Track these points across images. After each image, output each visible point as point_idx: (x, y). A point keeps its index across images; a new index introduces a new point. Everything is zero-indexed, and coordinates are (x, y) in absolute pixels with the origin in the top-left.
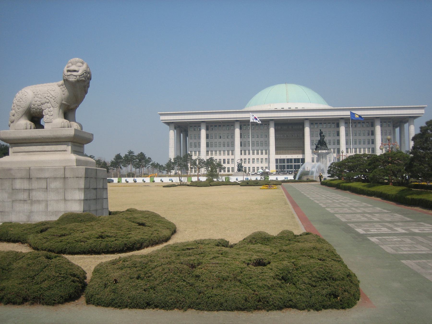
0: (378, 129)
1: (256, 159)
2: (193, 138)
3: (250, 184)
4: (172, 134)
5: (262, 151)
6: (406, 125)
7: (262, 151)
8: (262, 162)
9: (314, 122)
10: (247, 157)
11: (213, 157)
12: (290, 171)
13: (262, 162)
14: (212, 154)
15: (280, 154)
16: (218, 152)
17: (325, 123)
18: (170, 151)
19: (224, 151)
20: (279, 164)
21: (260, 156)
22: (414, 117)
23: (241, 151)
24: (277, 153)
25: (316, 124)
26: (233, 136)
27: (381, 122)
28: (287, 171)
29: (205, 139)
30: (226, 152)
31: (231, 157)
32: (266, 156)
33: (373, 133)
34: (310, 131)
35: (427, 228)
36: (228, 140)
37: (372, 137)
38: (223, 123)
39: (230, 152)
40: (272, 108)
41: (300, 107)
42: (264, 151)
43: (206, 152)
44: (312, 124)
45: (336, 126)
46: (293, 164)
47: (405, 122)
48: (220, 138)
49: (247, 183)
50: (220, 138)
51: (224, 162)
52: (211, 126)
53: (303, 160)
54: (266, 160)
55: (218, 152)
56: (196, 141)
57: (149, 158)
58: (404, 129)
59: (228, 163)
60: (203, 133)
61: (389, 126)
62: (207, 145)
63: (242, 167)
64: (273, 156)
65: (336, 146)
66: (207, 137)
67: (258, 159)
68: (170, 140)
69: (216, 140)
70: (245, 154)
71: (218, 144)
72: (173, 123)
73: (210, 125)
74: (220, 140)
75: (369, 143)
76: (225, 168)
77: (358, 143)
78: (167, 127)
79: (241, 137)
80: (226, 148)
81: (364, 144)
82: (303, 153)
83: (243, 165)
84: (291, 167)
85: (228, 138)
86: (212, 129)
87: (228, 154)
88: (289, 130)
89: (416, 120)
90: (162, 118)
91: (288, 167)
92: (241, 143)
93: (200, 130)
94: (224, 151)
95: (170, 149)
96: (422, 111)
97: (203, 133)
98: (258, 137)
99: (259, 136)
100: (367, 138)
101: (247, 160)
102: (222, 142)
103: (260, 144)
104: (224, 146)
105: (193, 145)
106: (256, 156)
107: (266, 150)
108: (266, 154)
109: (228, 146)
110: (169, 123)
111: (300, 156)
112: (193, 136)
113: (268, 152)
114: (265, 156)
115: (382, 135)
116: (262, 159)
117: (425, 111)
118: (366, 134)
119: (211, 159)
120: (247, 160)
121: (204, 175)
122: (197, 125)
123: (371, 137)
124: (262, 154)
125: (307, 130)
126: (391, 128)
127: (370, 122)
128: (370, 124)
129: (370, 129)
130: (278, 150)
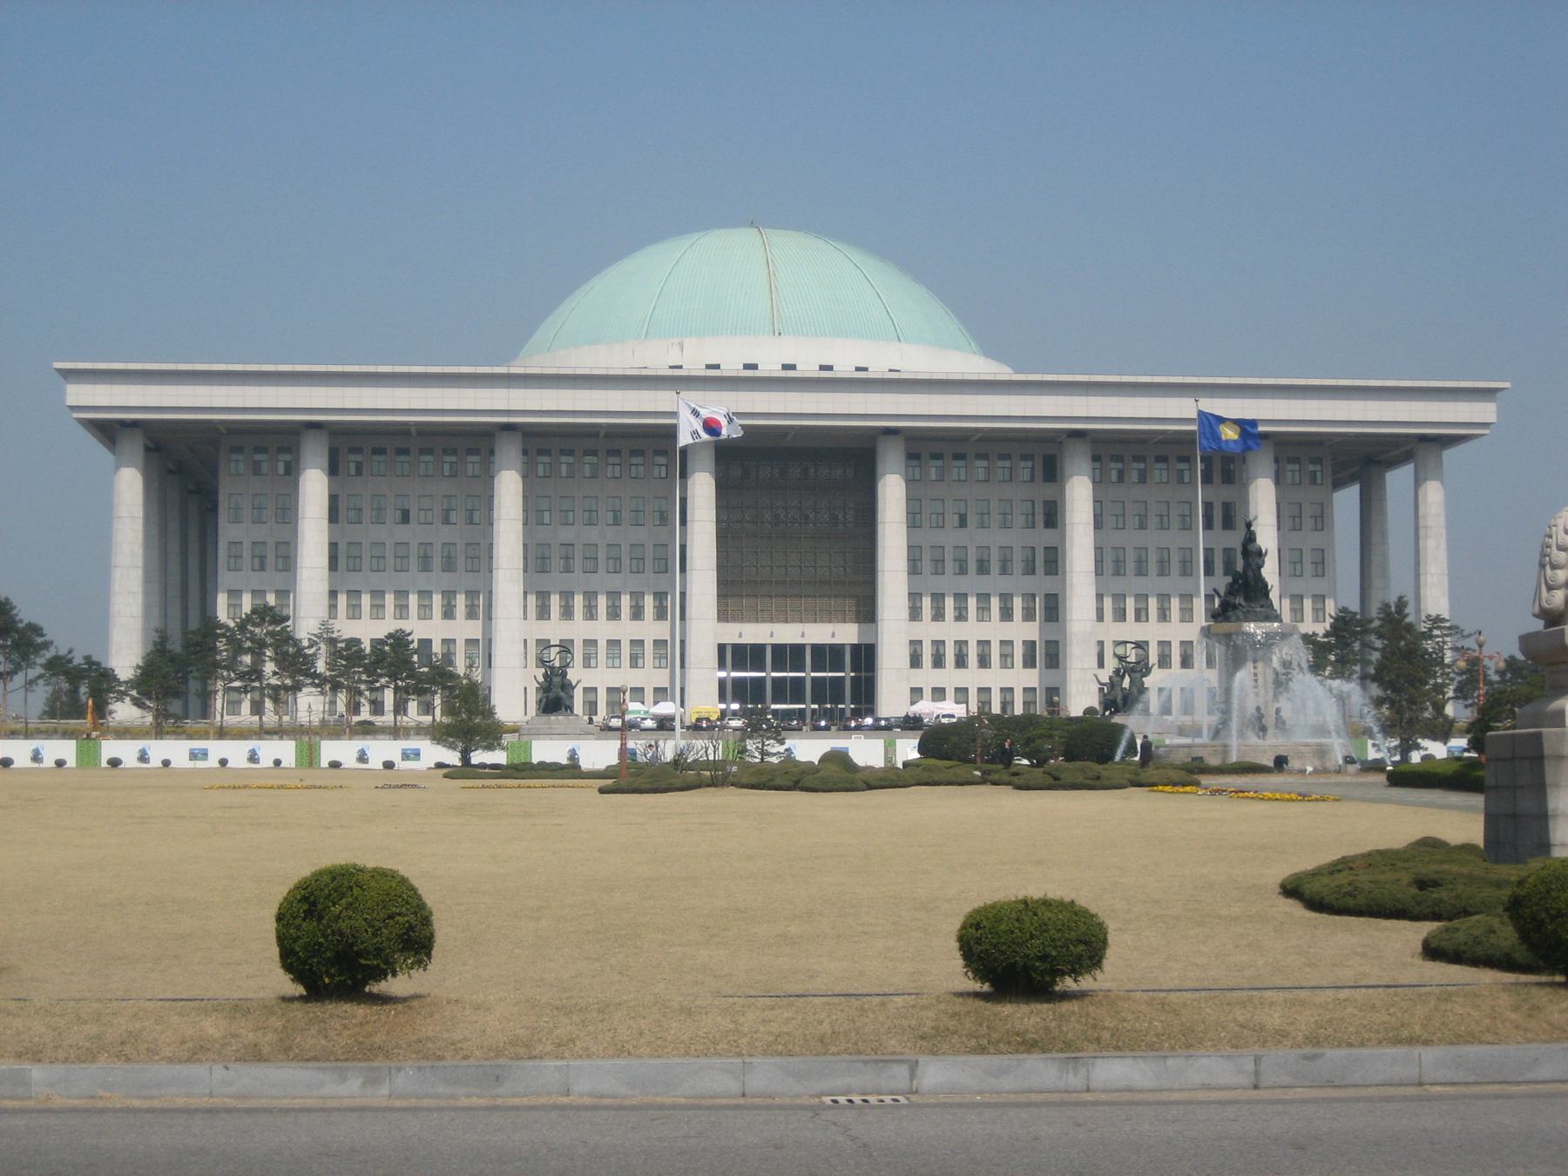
1: (602, 645)
4: (129, 487)
5: (637, 597)
6: (1398, 479)
7: (637, 597)
8: (635, 661)
9: (931, 449)
10: (950, 631)
11: (406, 625)
14: (402, 610)
16: (389, 599)
17: (984, 456)
19: (425, 594)
21: (626, 629)
23: (333, 594)
24: (725, 614)
25: (937, 456)
26: (288, 513)
29: (325, 522)
32: (660, 630)
33: (1053, 516)
34: (1097, 502)
36: (444, 534)
39: (1175, 603)
40: (656, 358)
41: (879, 366)
42: (461, 601)
43: (326, 597)
45: (1039, 473)
47: (1393, 463)
48: (405, 518)
49: (633, 778)
50: (405, 518)
52: (356, 450)
53: (865, 656)
54: (676, 646)
60: (314, 486)
61: (1313, 481)
63: (567, 687)
64: (707, 630)
65: (1041, 583)
67: (614, 644)
70: (938, 615)
71: (389, 553)
73: (357, 447)
74: (403, 533)
77: (1153, 566)
78: (93, 447)
79: (333, 516)
80: (438, 579)
81: (1004, 571)
82: (867, 612)
83: (572, 675)
85: (446, 521)
86: (359, 466)
88: (801, 493)
89: (1450, 455)
90: (81, 395)
91: (782, 690)
92: (333, 546)
94: (425, 594)
96: (1484, 412)
97: (314, 486)
98: (616, 523)
99: (626, 515)
100: (1018, 538)
103: (626, 561)
104: (425, 566)
105: (247, 554)
107: (472, 594)
108: (471, 614)
109: (449, 566)
110: (109, 431)
111: (846, 633)
113: (673, 605)
114: (651, 629)
115: (1098, 524)
116: (638, 643)
117: (1500, 413)
118: (1019, 520)
119: (399, 640)
122: (277, 443)
124: (637, 614)
125: (892, 492)
130: (735, 592)
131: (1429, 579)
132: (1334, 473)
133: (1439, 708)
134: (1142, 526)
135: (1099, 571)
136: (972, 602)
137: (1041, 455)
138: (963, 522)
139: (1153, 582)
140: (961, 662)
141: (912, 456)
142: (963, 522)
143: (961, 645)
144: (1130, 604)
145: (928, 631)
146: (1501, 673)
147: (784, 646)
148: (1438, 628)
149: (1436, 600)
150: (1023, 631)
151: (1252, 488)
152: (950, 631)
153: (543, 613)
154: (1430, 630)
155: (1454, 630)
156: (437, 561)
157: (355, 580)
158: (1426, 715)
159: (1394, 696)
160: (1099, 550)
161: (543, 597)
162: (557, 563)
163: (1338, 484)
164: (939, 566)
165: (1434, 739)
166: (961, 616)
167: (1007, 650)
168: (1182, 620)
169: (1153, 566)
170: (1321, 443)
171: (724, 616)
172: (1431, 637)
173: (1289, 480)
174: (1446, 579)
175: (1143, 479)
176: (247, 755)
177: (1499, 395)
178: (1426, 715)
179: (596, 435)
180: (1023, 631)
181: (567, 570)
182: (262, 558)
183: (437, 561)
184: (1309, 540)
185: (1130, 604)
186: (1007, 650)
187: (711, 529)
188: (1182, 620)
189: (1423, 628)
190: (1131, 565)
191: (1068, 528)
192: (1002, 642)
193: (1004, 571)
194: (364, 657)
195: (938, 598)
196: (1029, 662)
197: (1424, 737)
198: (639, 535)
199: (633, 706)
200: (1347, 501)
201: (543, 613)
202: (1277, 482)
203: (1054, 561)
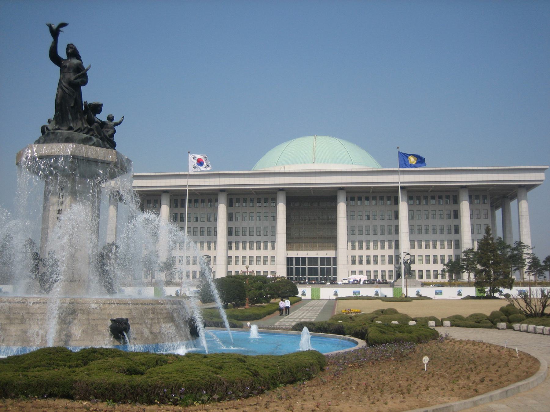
0: (465, 207)
1: (255, 258)
6: (513, 204)
8: (265, 263)
9: (357, 195)
10: (364, 252)
12: (313, 279)
13: (265, 263)
15: (296, 249)
20: (332, 267)
22: (528, 187)
27: (470, 197)
28: (309, 279)
30: (205, 245)
31: (269, 253)
33: (457, 215)
34: (409, 210)
37: (455, 222)
38: (202, 195)
44: (353, 199)
46: (294, 267)
47: (512, 198)
50: (197, 220)
59: (368, 262)
62: (230, 232)
66: (230, 217)
67: (258, 257)
74: (367, 223)
75: (449, 232)
77: (431, 231)
81: (442, 233)
82: (336, 248)
84: (316, 272)
85: (209, 220)
87: (368, 248)
93: (276, 206)
96: (540, 176)
97: (222, 209)
98: (260, 220)
99: (262, 218)
101: (241, 258)
102: (199, 228)
106: (255, 253)
116: (266, 257)
120: (241, 258)
121: (468, 284)
123: (454, 222)
127: (449, 195)
128: (452, 199)
131: (524, 233)
134: (427, 218)
135: (472, 233)
136: (372, 244)
137: (388, 195)
138: (368, 218)
139: (431, 236)
140: (368, 262)
141: (410, 198)
142: (368, 218)
143: (435, 256)
144: (424, 244)
145: (357, 253)
146: (544, 262)
147: (312, 258)
150: (389, 252)
151: (461, 204)
152: (364, 252)
153: (353, 247)
156: (205, 233)
157: (238, 239)
160: (472, 225)
161: (353, 243)
162: (357, 232)
163: (497, 208)
164: (361, 232)
166: (420, 247)
167: (383, 258)
168: (441, 248)
169: (431, 231)
171: (288, 248)
174: (529, 232)
175: (427, 204)
176: (457, 293)
177: (545, 171)
179: (427, 191)
180: (389, 252)
181: (245, 235)
182: (203, 232)
183: (205, 233)
185: (424, 244)
186: (383, 258)
187: (284, 220)
188: (441, 248)
190: (423, 231)
191: (461, 217)
192: (382, 256)
193: (382, 233)
194: (478, 263)
195: (420, 242)
196: (390, 262)
198: (267, 224)
199: (56, 276)
200: (499, 213)
201: (353, 247)
203: (457, 230)
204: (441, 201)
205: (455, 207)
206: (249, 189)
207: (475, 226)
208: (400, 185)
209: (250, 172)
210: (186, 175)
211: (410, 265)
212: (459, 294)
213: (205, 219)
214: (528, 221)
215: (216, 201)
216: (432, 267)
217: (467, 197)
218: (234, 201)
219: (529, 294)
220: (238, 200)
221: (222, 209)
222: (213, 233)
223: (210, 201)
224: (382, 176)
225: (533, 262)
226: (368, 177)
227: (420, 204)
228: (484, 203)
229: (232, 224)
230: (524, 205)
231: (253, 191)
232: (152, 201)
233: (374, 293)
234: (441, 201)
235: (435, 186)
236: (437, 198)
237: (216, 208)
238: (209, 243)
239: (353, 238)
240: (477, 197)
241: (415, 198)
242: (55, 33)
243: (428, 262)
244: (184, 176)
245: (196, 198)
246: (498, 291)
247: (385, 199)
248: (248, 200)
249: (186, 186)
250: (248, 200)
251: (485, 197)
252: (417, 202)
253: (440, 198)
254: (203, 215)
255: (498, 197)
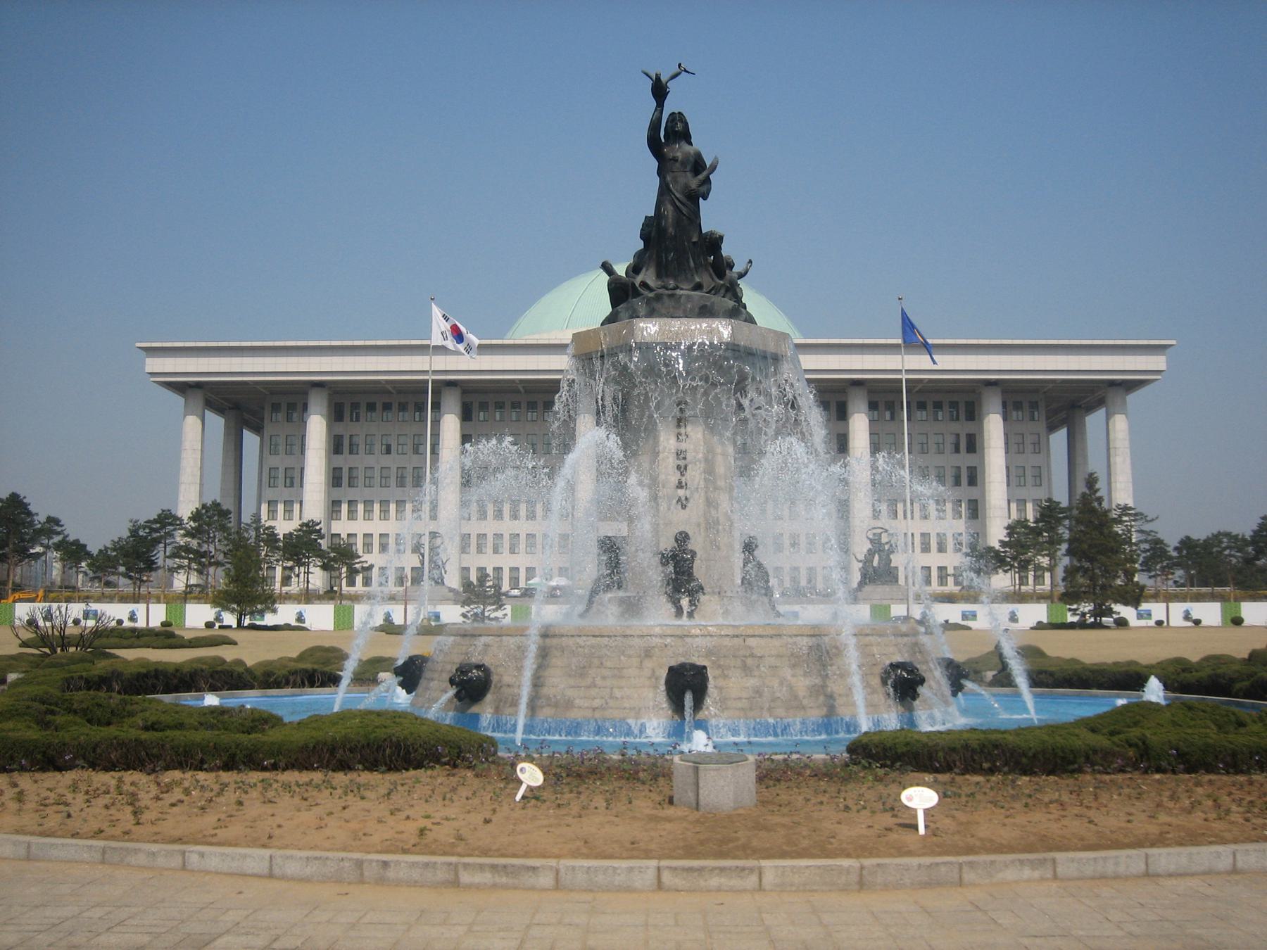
0: (994, 427)
1: (523, 537)
2: (281, 448)
3: (185, 839)
6: (1094, 421)
10: (490, 527)
16: (377, 507)
18: (181, 498)
22: (1129, 385)
26: (298, 445)
27: (1004, 405)
33: (973, 444)
35: (1251, 856)
37: (969, 460)
38: (399, 392)
47: (1090, 409)
48: (388, 451)
50: (388, 451)
51: (368, 547)
55: (377, 507)
56: (290, 461)
57: (50, 520)
58: (1083, 433)
59: (941, 549)
62: (335, 478)
66: (336, 445)
68: (184, 455)
69: (370, 460)
72: (198, 385)
73: (352, 402)
74: (387, 461)
76: (371, 567)
78: (178, 400)
80: (395, 492)
87: (515, 516)
89: (1133, 398)
90: (156, 365)
95: (182, 488)
96: (1157, 362)
97: (317, 428)
100: (951, 460)
101: (490, 538)
102: (377, 468)
110: (181, 388)
112: (281, 441)
118: (949, 447)
120: (490, 538)
123: (965, 460)
126: (1041, 426)
127: (954, 403)
129: (964, 428)
132: (1048, 418)
133: (1129, 574)
141: (873, 406)
146: (1176, 549)
148: (1126, 515)
149: (1121, 491)
151: (986, 421)
154: (1120, 516)
155: (1138, 516)
157: (352, 493)
158: (1119, 582)
159: (1087, 565)
163: (1052, 428)
165: (1126, 604)
170: (1036, 391)
172: (1121, 522)
173: (1014, 417)
176: (1182, 615)
177: (1168, 351)
178: (1119, 582)
184: (1030, 460)
189: (1114, 515)
197: (1116, 602)
200: (1059, 439)
202: (1005, 419)
203: (974, 477)
204: (940, 413)
205: (969, 427)
206: (513, 381)
207: (1013, 470)
208: (904, 377)
209: (506, 342)
210: (428, 346)
211: (888, 555)
212: (1013, 618)
213: (409, 448)
214: (1128, 461)
215: (305, 408)
216: (934, 560)
217: (863, 405)
218: (476, 406)
219: (269, 619)
220: (484, 406)
221: (317, 428)
222: (297, 480)
223: (532, 406)
224: (848, 357)
225: (1152, 549)
226: (854, 356)
227: (892, 418)
228: (1032, 419)
229: (339, 461)
230: (1120, 424)
231: (520, 387)
232: (284, 407)
233: (295, 617)
234: (940, 413)
235: (930, 380)
236: (930, 406)
237: (303, 423)
238: (288, 504)
239: (1022, 493)
240: (1018, 406)
241: (882, 406)
242: (660, 91)
243: (926, 549)
244: (422, 349)
245: (955, 399)
246: (1110, 612)
247: (491, 408)
248: (508, 405)
249: (899, 371)
250: (508, 405)
251: (1034, 405)
252: (888, 415)
253: (938, 405)
254: (402, 440)
255: (1060, 406)
